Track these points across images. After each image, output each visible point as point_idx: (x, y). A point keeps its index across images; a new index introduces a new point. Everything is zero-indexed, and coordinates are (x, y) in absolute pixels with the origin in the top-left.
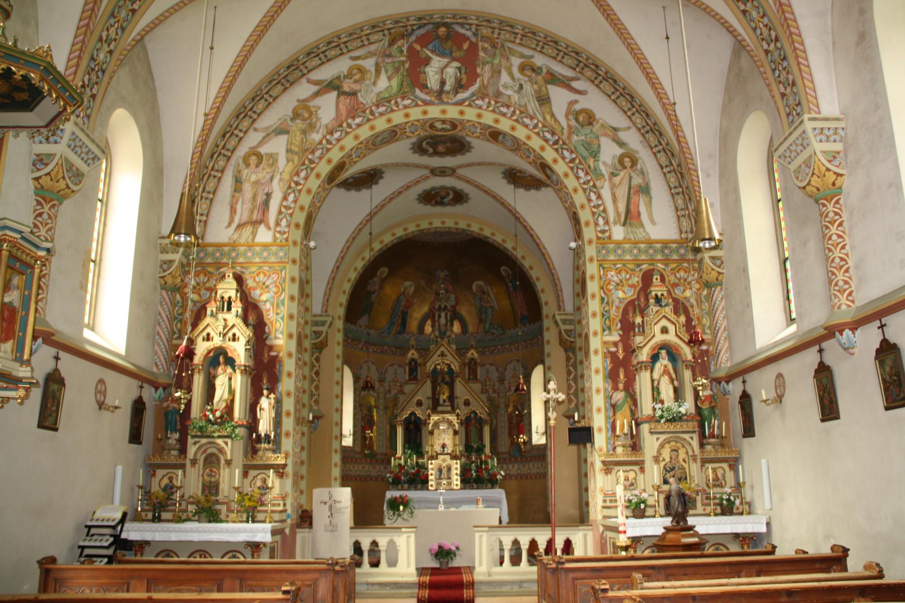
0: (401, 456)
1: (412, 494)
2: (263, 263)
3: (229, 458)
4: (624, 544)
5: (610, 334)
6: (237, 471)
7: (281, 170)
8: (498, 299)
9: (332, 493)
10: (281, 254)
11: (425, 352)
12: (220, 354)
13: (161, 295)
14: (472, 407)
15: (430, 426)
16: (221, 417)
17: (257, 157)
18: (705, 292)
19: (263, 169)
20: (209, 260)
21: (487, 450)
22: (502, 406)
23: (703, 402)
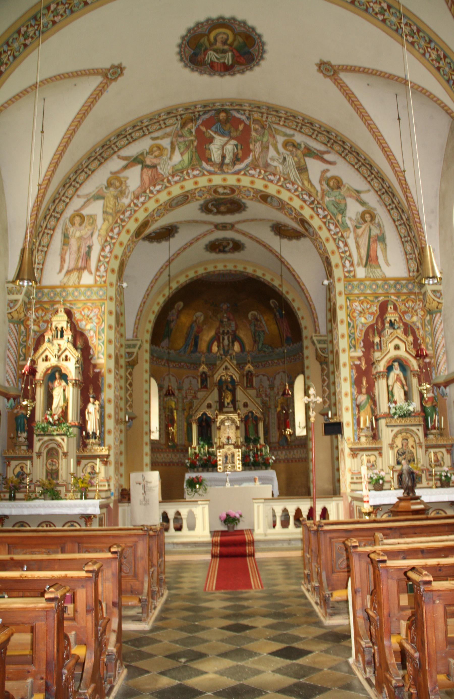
0: (196, 446)
1: (205, 475)
2: (87, 300)
4: (368, 511)
5: (355, 350)
6: (72, 460)
7: (99, 227)
11: (212, 366)
12: (56, 371)
13: (10, 327)
14: (250, 408)
16: (59, 420)
17: (80, 218)
18: (428, 318)
19: (85, 227)
20: (46, 299)
21: (262, 441)
22: (273, 407)
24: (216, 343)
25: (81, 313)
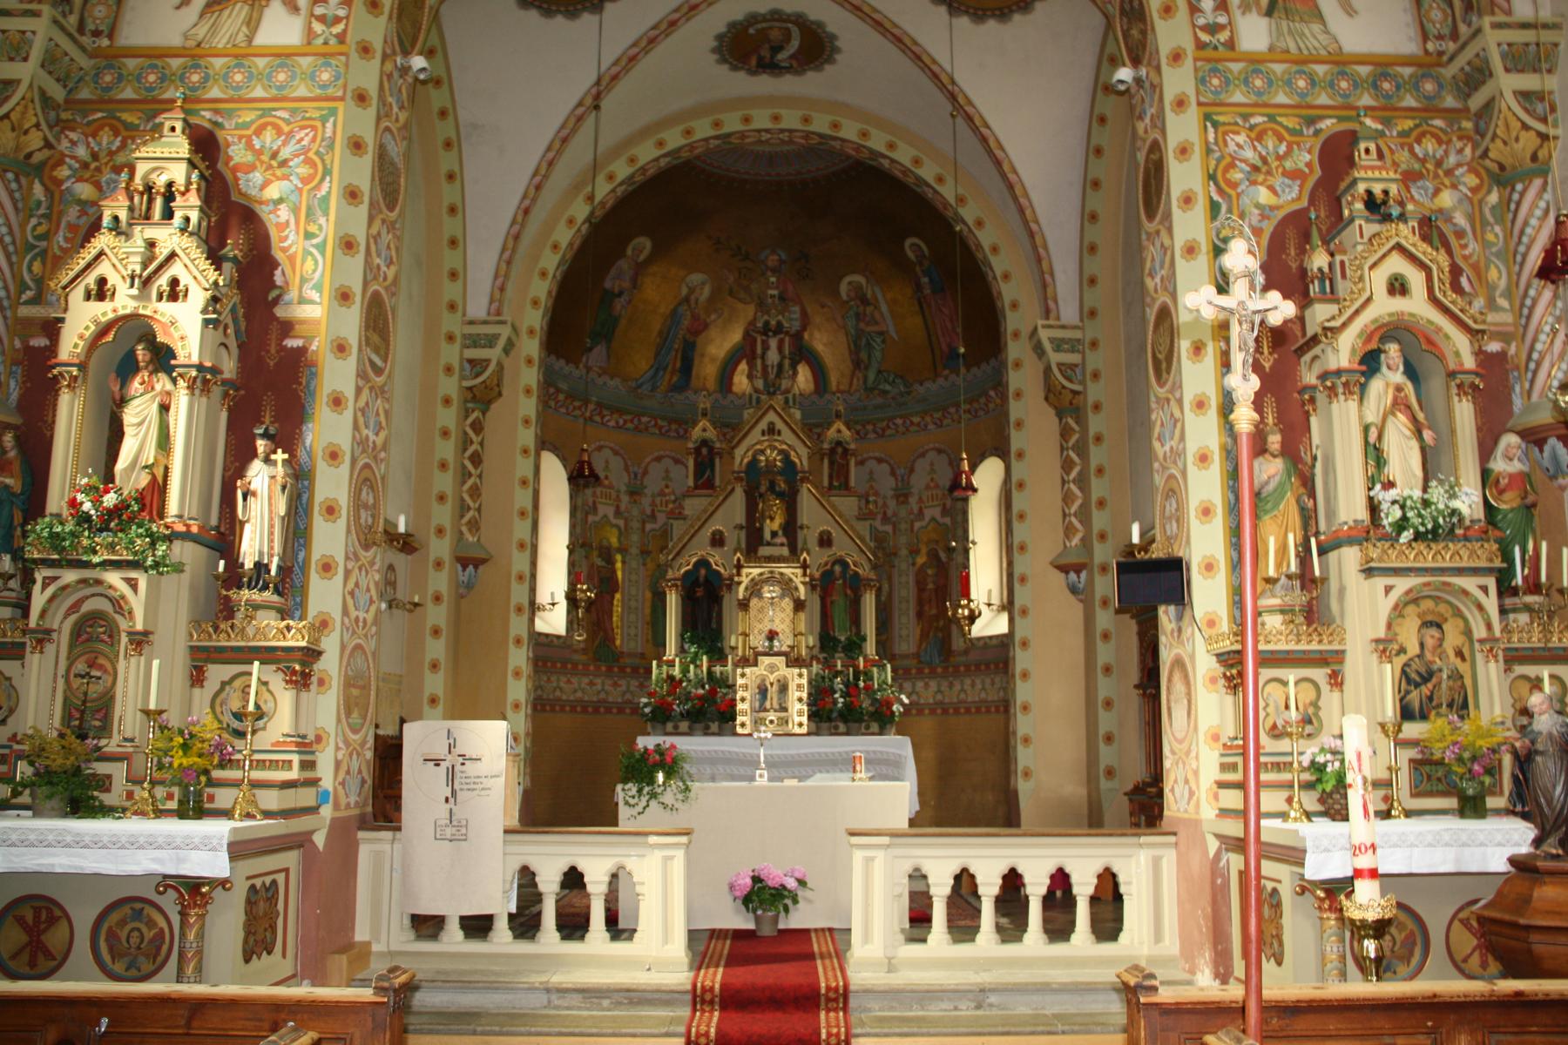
0: (674, 658)
1: (689, 745)
3: (139, 627)
4: (1371, 916)
8: (895, 312)
9: (455, 733)
10: (325, 76)
11: (732, 428)
14: (837, 550)
15: (742, 588)
18: (1493, 198)
20: (128, 93)
21: (870, 648)
22: (904, 552)
23: (1501, 492)
24: (743, 366)
25: (250, 146)
